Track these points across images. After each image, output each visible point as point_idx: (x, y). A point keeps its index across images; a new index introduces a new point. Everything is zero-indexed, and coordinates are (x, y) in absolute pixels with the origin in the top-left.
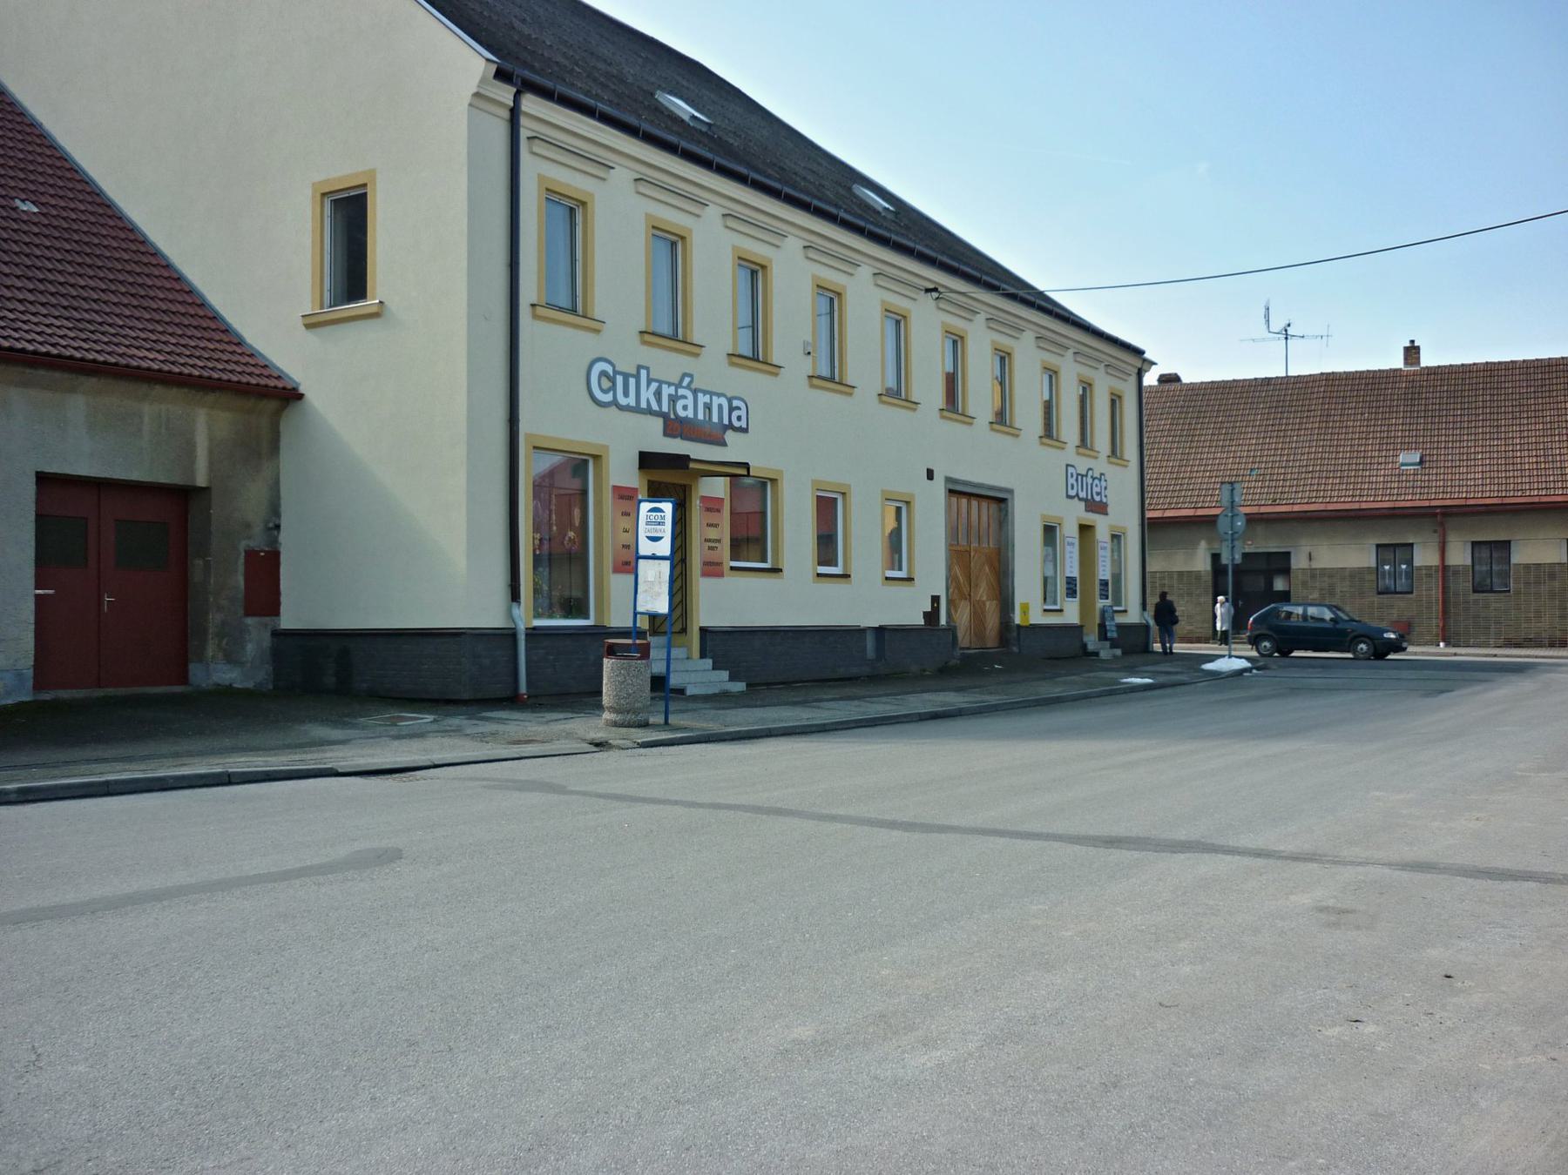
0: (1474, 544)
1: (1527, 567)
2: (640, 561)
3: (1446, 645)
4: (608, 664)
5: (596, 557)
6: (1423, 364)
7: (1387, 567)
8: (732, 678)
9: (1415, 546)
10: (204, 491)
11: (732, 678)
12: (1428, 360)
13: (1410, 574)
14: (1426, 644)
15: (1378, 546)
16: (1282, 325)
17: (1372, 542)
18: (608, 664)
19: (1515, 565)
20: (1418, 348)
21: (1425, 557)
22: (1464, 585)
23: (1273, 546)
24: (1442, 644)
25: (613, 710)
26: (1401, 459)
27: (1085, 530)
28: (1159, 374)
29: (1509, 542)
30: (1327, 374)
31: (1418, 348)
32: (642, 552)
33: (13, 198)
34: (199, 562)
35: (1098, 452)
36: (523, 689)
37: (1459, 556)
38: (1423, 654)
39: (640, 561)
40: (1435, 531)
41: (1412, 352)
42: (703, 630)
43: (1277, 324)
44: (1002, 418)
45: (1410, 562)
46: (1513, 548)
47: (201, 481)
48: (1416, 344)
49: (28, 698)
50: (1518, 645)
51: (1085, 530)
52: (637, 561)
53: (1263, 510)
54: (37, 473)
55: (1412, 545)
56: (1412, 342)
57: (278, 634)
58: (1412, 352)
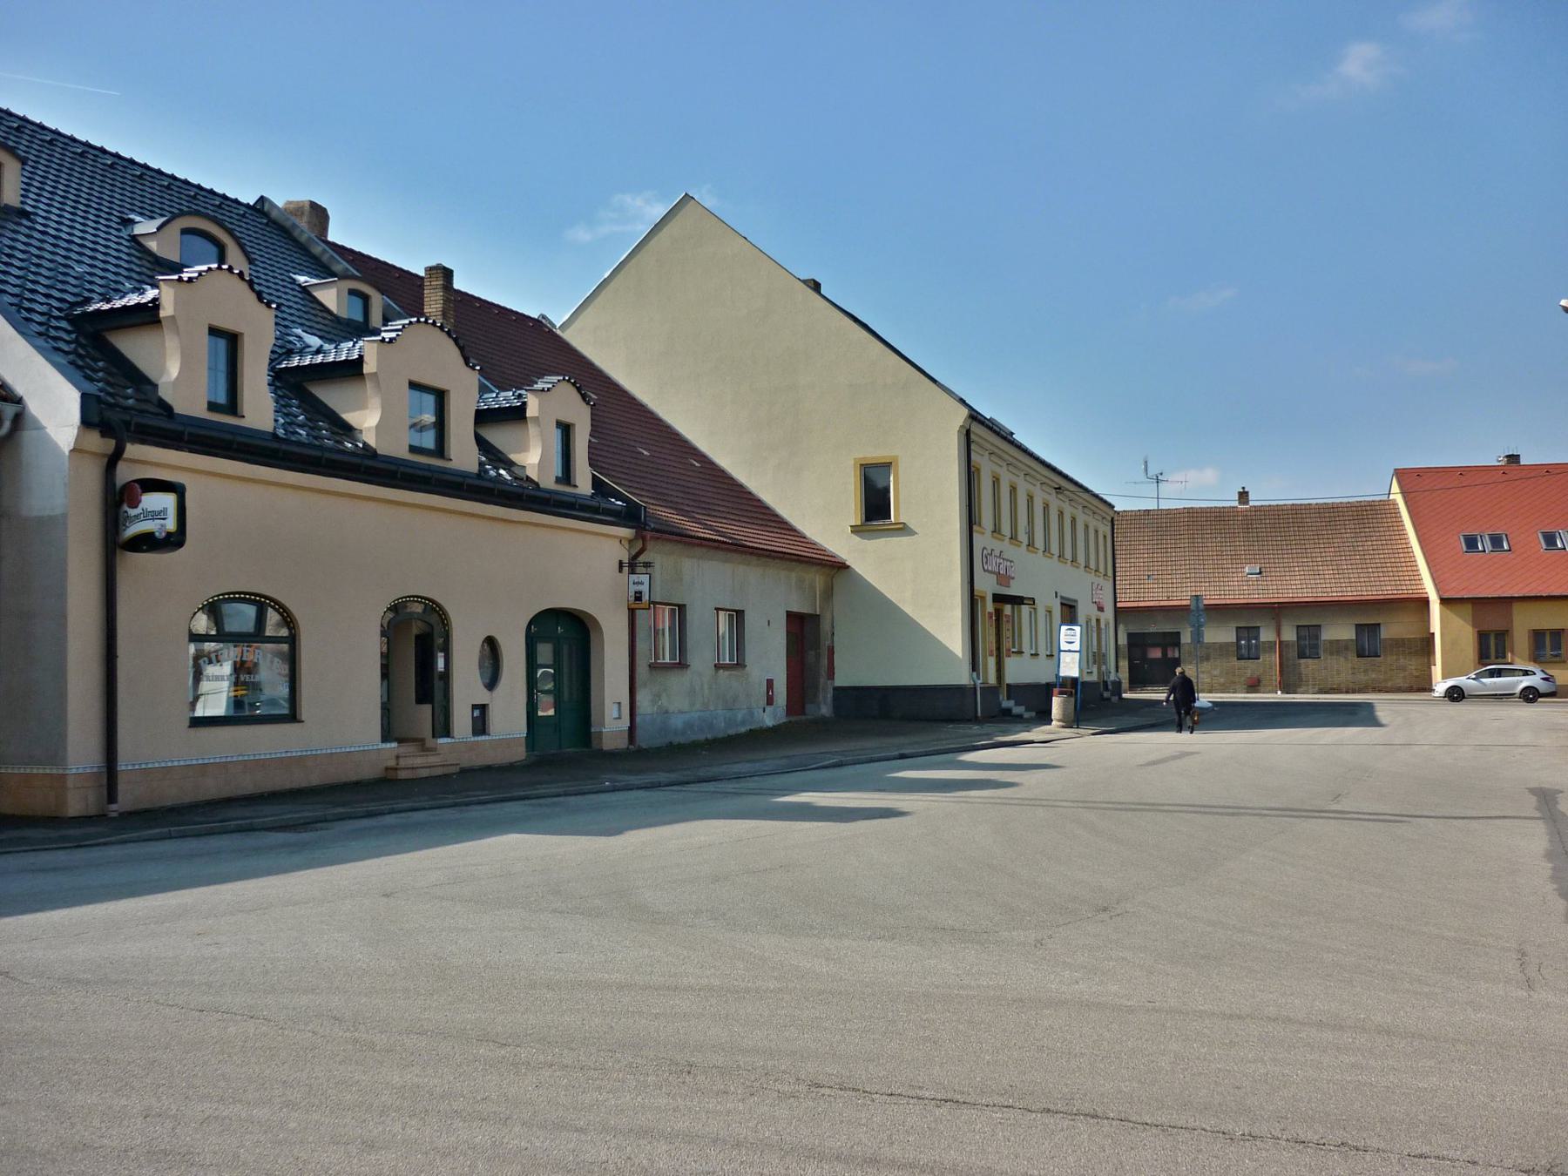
0: (1298, 626)
1: (1331, 642)
2: (1062, 653)
3: (1282, 693)
4: (540, 713)
5: (982, 649)
6: (1251, 503)
7: (1243, 642)
8: (1027, 710)
9: (1261, 630)
10: (819, 615)
11: (1027, 710)
12: (1255, 500)
13: (1257, 646)
14: (1269, 692)
15: (1238, 628)
16: (1158, 472)
17: (1233, 625)
18: (540, 713)
19: (1324, 641)
20: (1247, 493)
21: (1267, 635)
22: (1293, 653)
23: (1168, 628)
24: (1279, 692)
25: (1059, 721)
26: (1247, 570)
27: (1098, 621)
28: (439, 262)
29: (1320, 626)
30: (1188, 508)
31: (1247, 493)
32: (1062, 648)
33: (701, 467)
34: (813, 653)
35: (269, 375)
36: (979, 714)
37: (1289, 635)
38: (1241, 698)
39: (1062, 653)
40: (1273, 619)
41: (1243, 496)
42: (1007, 685)
43: (1153, 471)
44: (1074, 560)
45: (1257, 638)
46: (1322, 630)
47: (818, 613)
48: (1246, 490)
49: (785, 721)
50: (1326, 693)
51: (1098, 621)
52: (1059, 654)
53: (1162, 604)
54: (787, 611)
55: (1259, 627)
56: (1243, 488)
57: (836, 689)
58: (1243, 496)
